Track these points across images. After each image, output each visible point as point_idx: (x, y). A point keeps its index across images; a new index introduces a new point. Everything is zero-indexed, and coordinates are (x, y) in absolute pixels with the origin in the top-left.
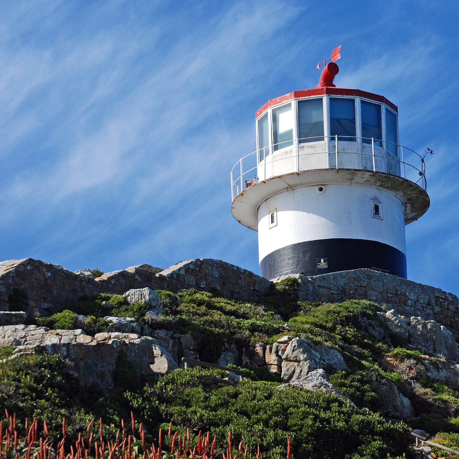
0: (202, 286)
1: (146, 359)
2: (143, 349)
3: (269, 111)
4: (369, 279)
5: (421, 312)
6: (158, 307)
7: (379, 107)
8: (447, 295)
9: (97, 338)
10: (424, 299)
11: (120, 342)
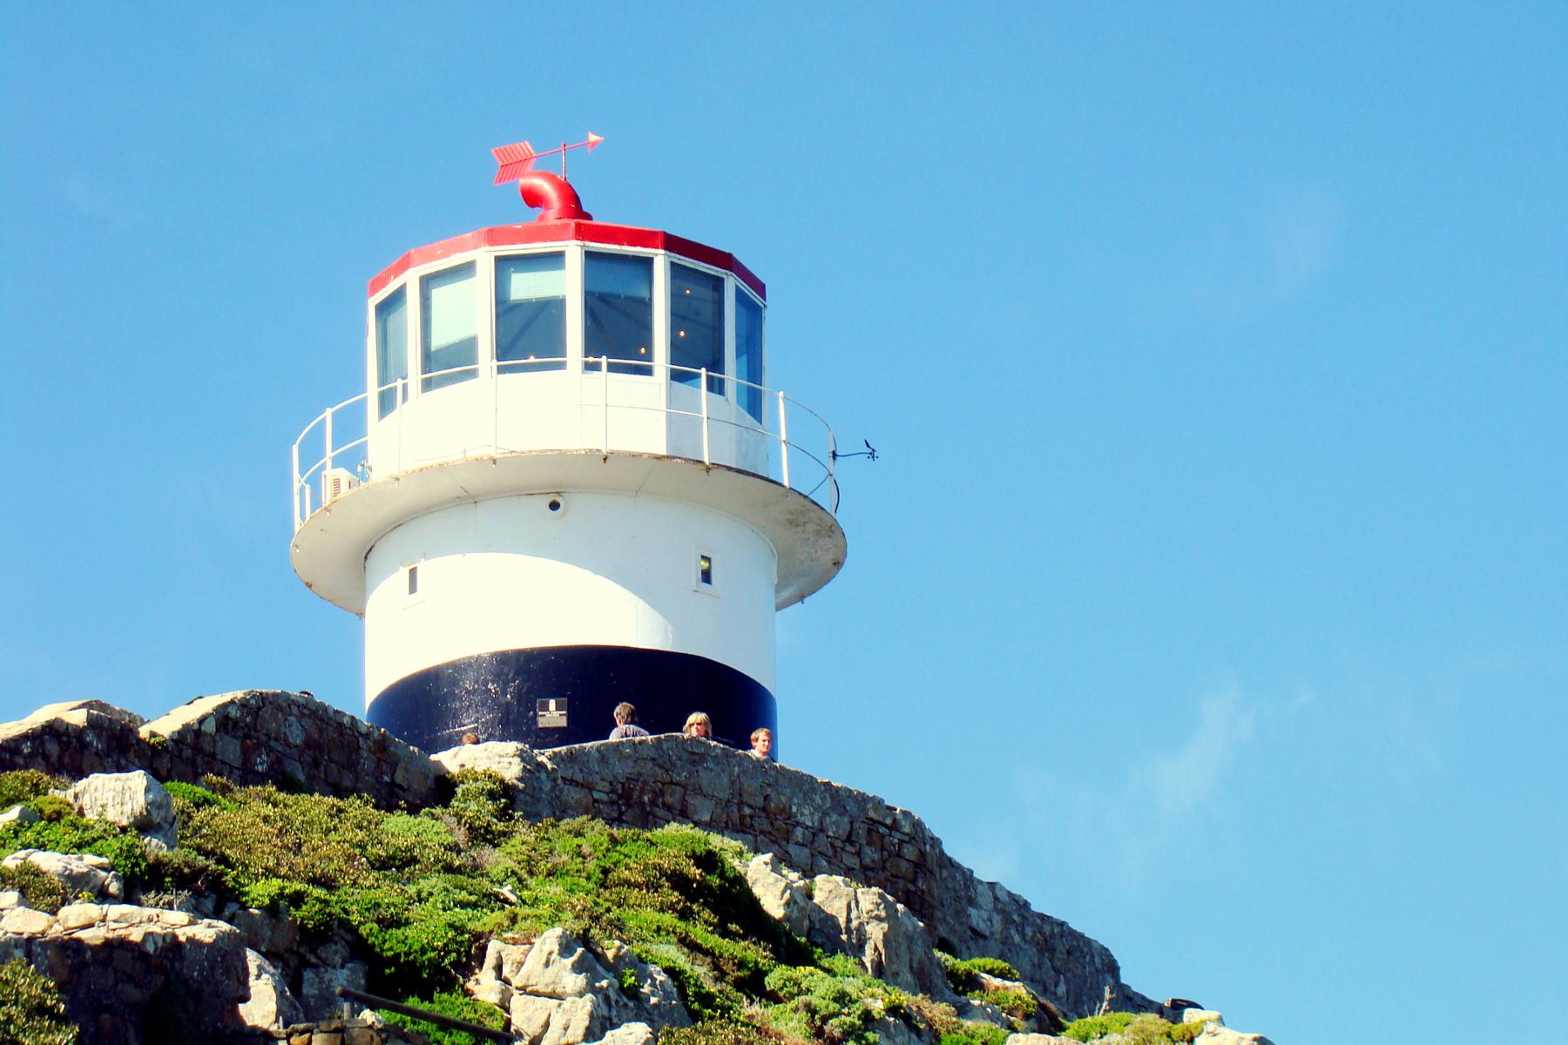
0: (260, 768)
1: (228, 984)
2: (223, 958)
3: (411, 279)
4: (693, 763)
5: (829, 862)
6: (166, 826)
7: (718, 283)
8: (899, 817)
9: (67, 918)
10: (836, 826)
11: (164, 936)
